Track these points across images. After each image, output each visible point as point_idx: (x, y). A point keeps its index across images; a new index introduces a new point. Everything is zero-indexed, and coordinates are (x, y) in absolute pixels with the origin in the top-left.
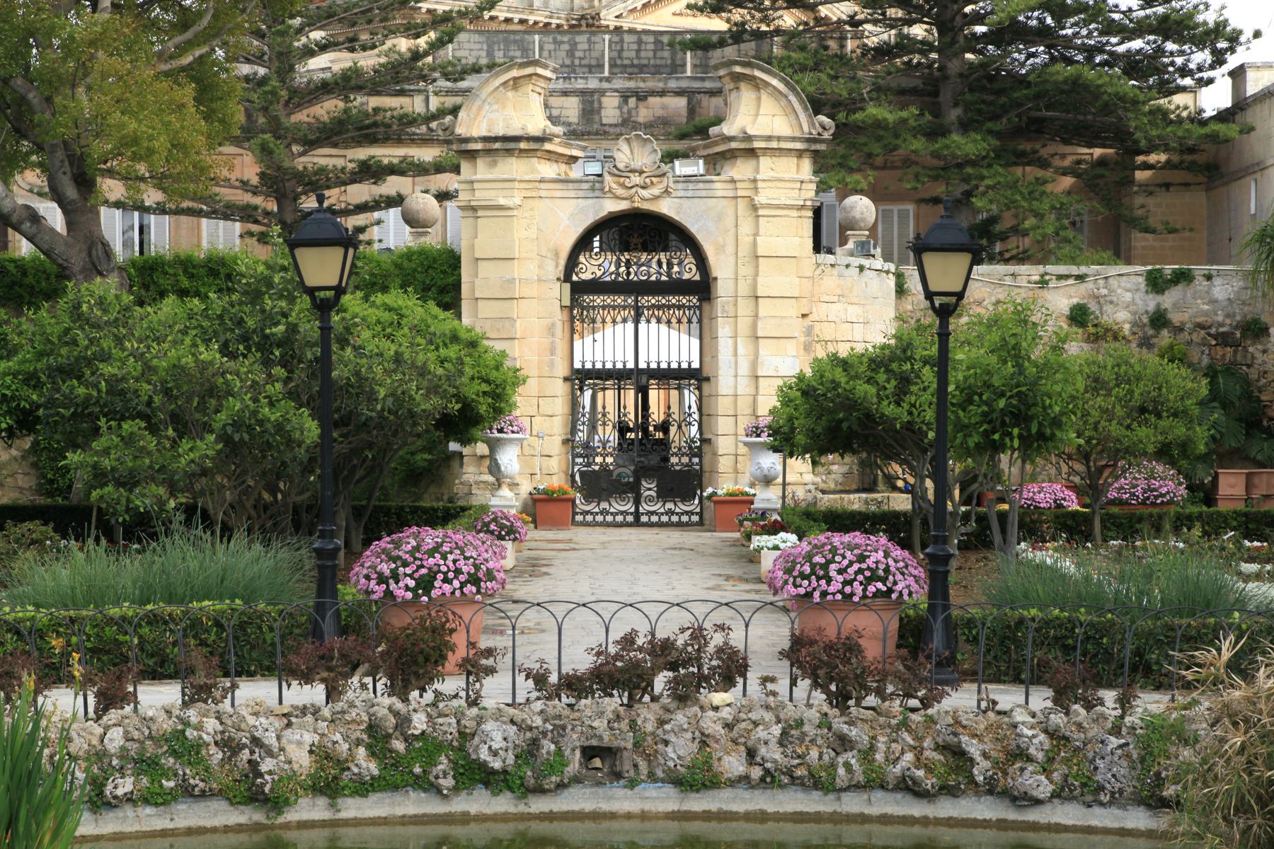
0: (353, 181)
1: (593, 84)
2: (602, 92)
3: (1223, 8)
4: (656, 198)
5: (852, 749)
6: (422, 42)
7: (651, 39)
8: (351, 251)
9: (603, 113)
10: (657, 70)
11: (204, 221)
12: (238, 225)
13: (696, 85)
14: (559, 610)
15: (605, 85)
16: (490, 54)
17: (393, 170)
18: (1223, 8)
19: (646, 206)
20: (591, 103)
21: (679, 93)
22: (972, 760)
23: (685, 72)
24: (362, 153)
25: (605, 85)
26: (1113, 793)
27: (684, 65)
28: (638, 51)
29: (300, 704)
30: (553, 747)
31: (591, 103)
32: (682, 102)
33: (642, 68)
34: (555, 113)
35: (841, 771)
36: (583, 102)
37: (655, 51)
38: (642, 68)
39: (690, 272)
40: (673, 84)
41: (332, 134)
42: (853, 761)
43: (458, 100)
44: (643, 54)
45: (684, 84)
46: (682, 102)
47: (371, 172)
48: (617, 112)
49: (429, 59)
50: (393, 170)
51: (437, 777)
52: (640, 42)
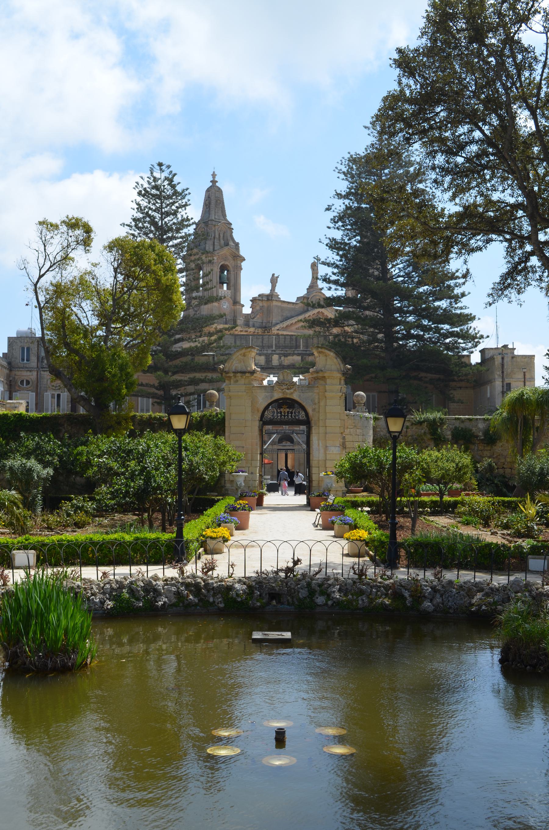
0: (189, 385)
1: (270, 352)
2: (273, 354)
3: (366, 127)
4: (292, 393)
5: (364, 594)
6: (213, 338)
7: (289, 337)
8: (189, 416)
9: (273, 362)
10: (291, 348)
11: (140, 398)
12: (151, 399)
13: (304, 352)
14: (261, 543)
15: (273, 352)
16: (235, 342)
17: (203, 381)
18: (366, 127)
19: (288, 396)
20: (269, 360)
21: (298, 355)
22: (406, 598)
23: (300, 348)
24: (192, 375)
25: (273, 352)
26: (454, 610)
27: (300, 346)
28: (285, 341)
29: (171, 577)
30: (259, 593)
31: (269, 360)
32: (299, 358)
33: (286, 347)
34: (257, 362)
35: (360, 602)
36: (266, 358)
37: (290, 341)
38: (286, 347)
39: (302, 416)
40: (296, 352)
41: (183, 369)
42: (364, 599)
43: (225, 357)
44: (286, 342)
45: (300, 352)
46: (299, 358)
47: (194, 382)
48: (277, 362)
49: (215, 344)
50: (203, 381)
51: (218, 603)
52: (285, 338)
